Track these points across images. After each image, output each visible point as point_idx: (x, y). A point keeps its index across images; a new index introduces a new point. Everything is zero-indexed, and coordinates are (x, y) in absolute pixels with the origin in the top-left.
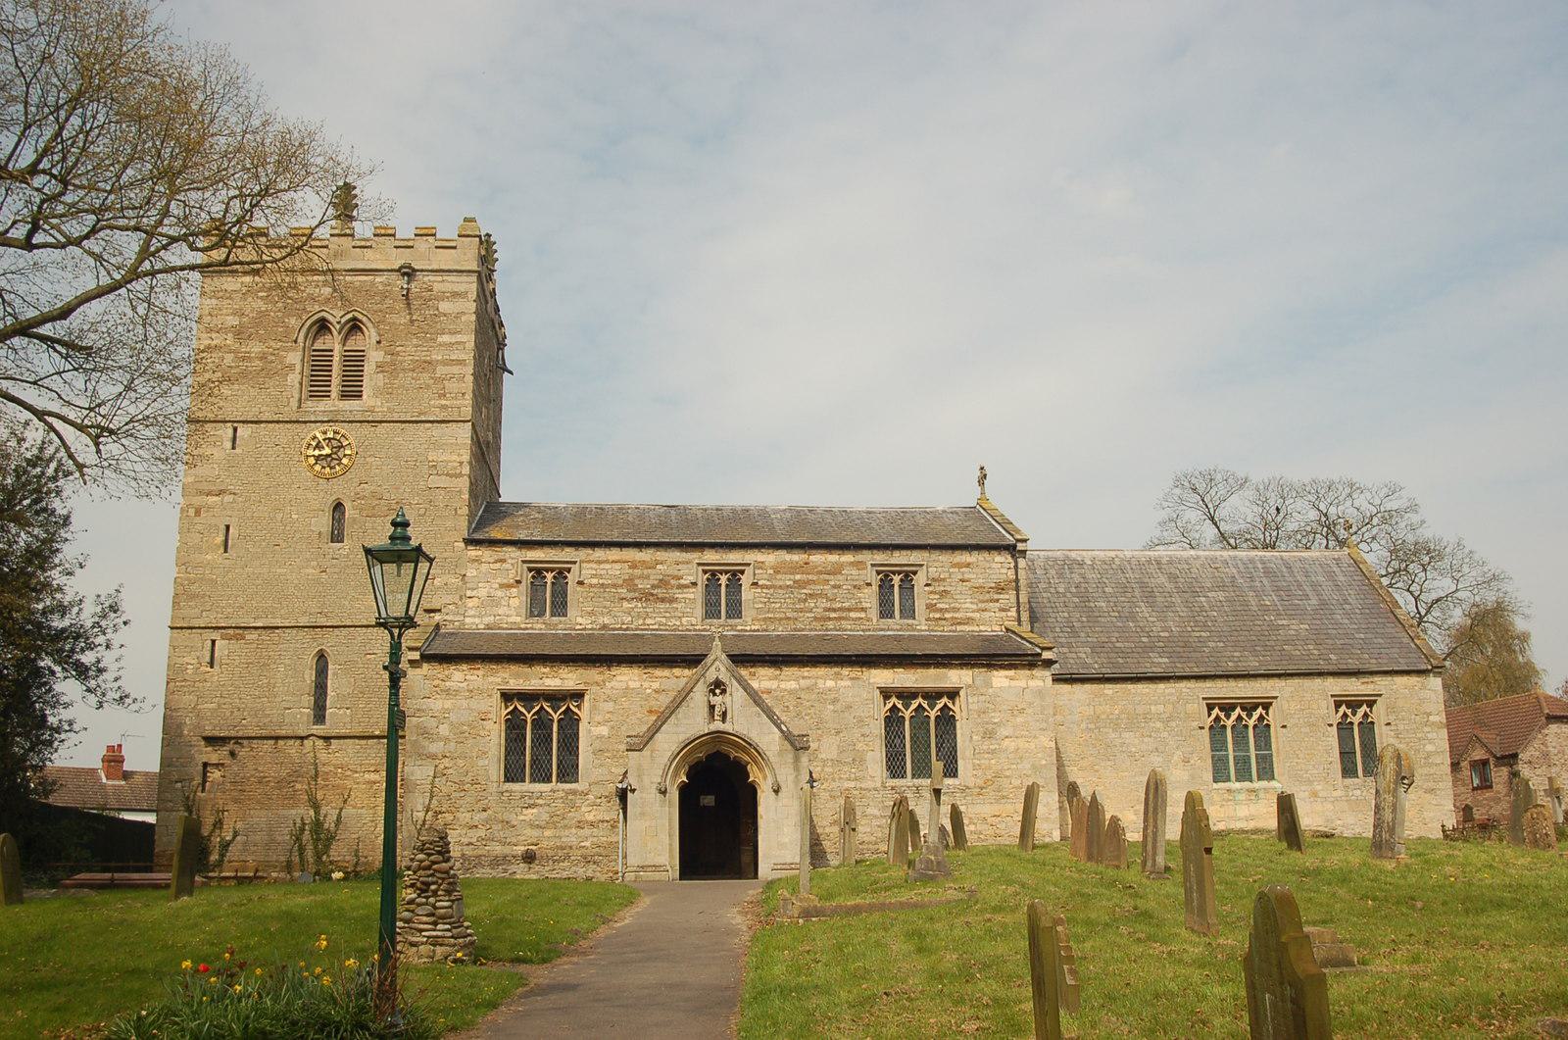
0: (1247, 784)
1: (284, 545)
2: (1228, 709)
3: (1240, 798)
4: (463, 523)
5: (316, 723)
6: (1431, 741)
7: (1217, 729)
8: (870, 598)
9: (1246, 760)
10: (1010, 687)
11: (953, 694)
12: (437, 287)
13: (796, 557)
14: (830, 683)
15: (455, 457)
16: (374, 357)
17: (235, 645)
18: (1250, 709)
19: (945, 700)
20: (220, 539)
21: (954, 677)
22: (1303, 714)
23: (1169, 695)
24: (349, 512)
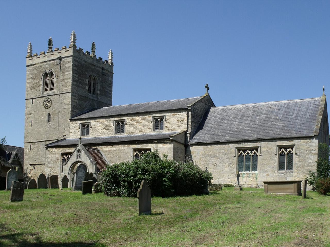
0: (248, 172)
1: (41, 124)
3: (244, 176)
4: (70, 116)
5: (281, 166)
6: (311, 159)
7: (240, 157)
8: (151, 125)
9: (249, 165)
10: (163, 147)
12: (66, 61)
14: (123, 148)
15: (68, 101)
16: (55, 80)
17: (34, 146)
18: (252, 149)
19: (290, 149)
20: (31, 124)
22: (268, 153)
23: (226, 147)
24: (51, 116)
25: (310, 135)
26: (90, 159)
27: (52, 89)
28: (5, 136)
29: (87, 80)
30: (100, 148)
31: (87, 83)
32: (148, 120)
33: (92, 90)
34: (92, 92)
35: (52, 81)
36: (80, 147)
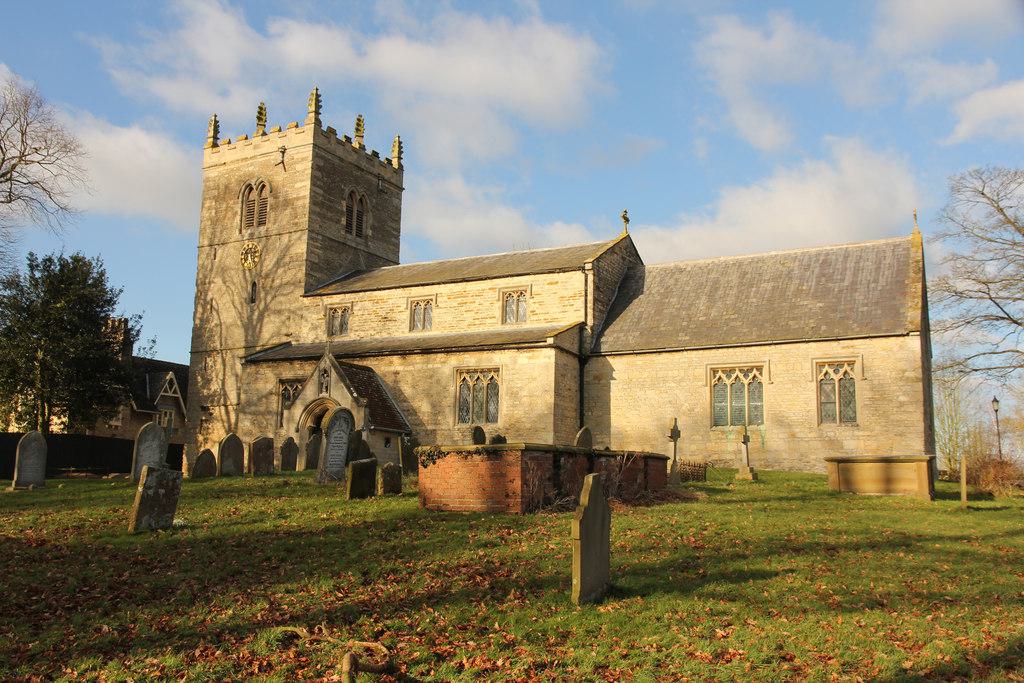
2: (729, 372)
19: (846, 367)
26: (352, 394)
27: (261, 223)
29: (344, 203)
30: (369, 363)
31: (345, 209)
33: (354, 228)
34: (354, 232)
36: (326, 362)
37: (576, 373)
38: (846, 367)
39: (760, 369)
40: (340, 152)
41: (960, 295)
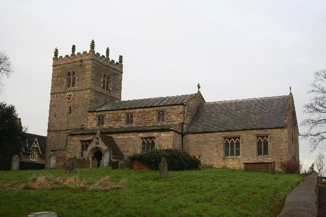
2: (229, 139)
5: (259, 153)
6: (282, 146)
7: (227, 144)
11: (154, 138)
13: (142, 110)
16: (77, 78)
18: (235, 139)
19: (265, 138)
21: (155, 134)
22: (248, 140)
25: (280, 126)
28: (93, 42)
29: (102, 79)
30: (114, 136)
32: (153, 112)
35: (74, 79)
36: (98, 136)
37: (181, 139)
38: (265, 138)
39: (239, 138)
40: (101, 61)
41: (317, 110)
